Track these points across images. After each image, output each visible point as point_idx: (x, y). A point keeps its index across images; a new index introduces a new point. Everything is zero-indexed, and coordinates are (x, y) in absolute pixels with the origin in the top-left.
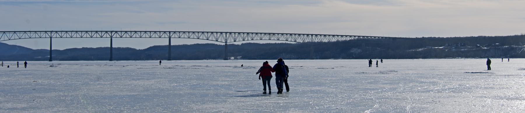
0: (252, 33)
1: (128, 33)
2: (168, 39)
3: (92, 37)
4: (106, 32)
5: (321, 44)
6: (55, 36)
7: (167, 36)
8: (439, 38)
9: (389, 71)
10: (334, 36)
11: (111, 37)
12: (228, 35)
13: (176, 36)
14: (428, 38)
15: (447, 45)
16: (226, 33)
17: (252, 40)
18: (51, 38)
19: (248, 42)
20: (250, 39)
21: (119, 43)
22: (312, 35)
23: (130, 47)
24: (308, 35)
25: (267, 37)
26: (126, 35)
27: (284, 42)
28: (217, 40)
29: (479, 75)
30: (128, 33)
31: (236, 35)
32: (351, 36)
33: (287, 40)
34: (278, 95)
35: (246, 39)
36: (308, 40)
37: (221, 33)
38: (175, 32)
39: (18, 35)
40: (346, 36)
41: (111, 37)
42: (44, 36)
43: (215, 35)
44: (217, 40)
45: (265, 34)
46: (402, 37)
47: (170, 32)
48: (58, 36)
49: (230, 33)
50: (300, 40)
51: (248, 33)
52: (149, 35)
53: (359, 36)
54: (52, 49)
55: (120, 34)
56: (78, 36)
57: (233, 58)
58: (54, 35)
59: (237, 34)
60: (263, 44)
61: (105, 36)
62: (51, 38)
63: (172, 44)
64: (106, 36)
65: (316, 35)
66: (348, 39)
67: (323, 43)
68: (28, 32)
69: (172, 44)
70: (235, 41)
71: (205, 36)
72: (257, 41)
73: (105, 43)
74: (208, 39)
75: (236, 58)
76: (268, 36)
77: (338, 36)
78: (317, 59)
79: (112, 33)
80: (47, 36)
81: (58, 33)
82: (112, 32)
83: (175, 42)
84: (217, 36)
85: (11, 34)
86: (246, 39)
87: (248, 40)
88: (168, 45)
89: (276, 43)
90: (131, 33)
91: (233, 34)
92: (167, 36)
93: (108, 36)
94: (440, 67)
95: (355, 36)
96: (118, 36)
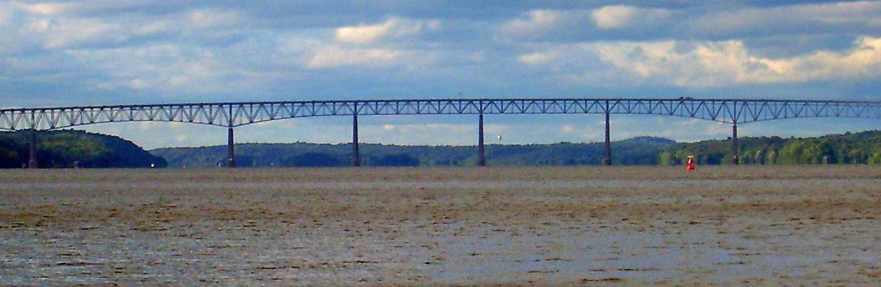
1: (369, 105)
2: (478, 116)
7: (348, 112)
11: (481, 112)
12: (738, 107)
26: (303, 110)
28: (12, 127)
30: (369, 105)
34: (827, 165)
35: (78, 122)
39: (855, 108)
41: (481, 112)
44: (12, 127)
49: (241, 104)
52: (332, 109)
54: (738, 136)
59: (215, 109)
64: (640, 109)
68: (667, 102)
69: (236, 140)
70: (72, 125)
76: (835, 107)
81: (515, 104)
84: (53, 117)
85: (759, 105)
86: (78, 122)
87: (82, 124)
90: (650, 104)
91: (247, 108)
92: (348, 112)
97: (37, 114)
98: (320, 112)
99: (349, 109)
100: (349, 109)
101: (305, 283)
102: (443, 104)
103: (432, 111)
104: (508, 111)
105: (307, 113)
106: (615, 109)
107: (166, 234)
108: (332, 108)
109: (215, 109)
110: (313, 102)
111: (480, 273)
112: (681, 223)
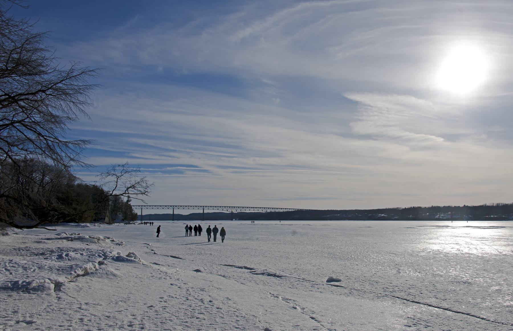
0: (245, 207)
2: (141, 209)
3: (163, 209)
4: (171, 206)
5: (275, 213)
6: (144, 208)
7: (202, 208)
8: (336, 210)
9: (44, 239)
10: (281, 209)
11: (173, 209)
13: (207, 209)
14: (339, 210)
15: (341, 214)
16: (232, 207)
17: (245, 210)
18: (142, 209)
19: (243, 211)
20: (244, 210)
21: (177, 212)
22: (275, 208)
23: (357, 209)
24: (273, 208)
25: (253, 209)
27: (261, 212)
29: (434, 228)
31: (228, 208)
32: (294, 209)
33: (262, 211)
36: (273, 211)
37: (230, 207)
38: (206, 206)
40: (292, 209)
41: (173, 209)
42: (138, 208)
43: (227, 208)
45: (252, 207)
46: (453, 205)
47: (203, 206)
48: (145, 208)
50: (269, 211)
51: (243, 207)
53: (298, 209)
54: (204, 212)
55: (178, 207)
56: (192, 208)
57: (234, 219)
58: (143, 208)
59: (228, 208)
60: (248, 213)
61: (170, 208)
62: (142, 209)
63: (175, 213)
65: (277, 208)
66: (293, 210)
67: (499, 206)
71: (226, 209)
72: (243, 211)
73: (170, 212)
74: (223, 210)
75: (236, 220)
77: (288, 209)
78: (277, 220)
79: (173, 207)
80: (140, 208)
82: (174, 206)
83: (206, 211)
87: (243, 211)
88: (172, 214)
89: (486, 205)
92: (202, 208)
93: (172, 208)
94: (127, 234)
95: (296, 209)
96: (177, 208)
97: (233, 208)
98: (190, 208)
99: (202, 208)
100: (202, 208)
101: (59, 330)
102: (199, 207)
103: (151, 208)
104: (185, 208)
105: (192, 208)
106: (205, 209)
107: (220, 245)
108: (188, 207)
109: (228, 208)
110: (189, 206)
111: (59, 199)
112: (77, 165)
